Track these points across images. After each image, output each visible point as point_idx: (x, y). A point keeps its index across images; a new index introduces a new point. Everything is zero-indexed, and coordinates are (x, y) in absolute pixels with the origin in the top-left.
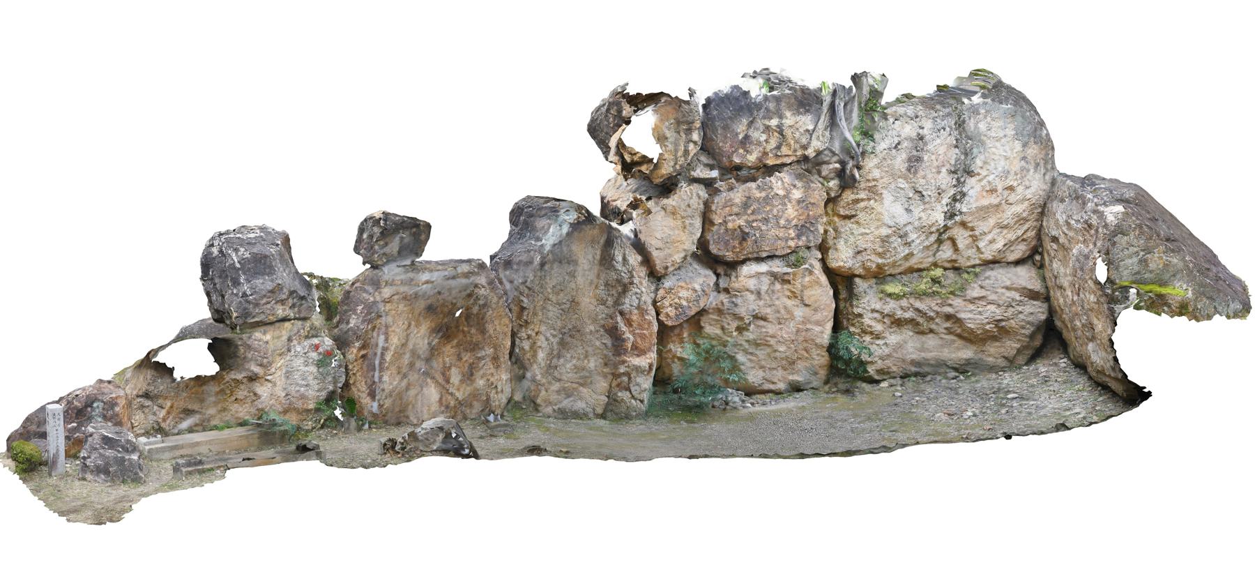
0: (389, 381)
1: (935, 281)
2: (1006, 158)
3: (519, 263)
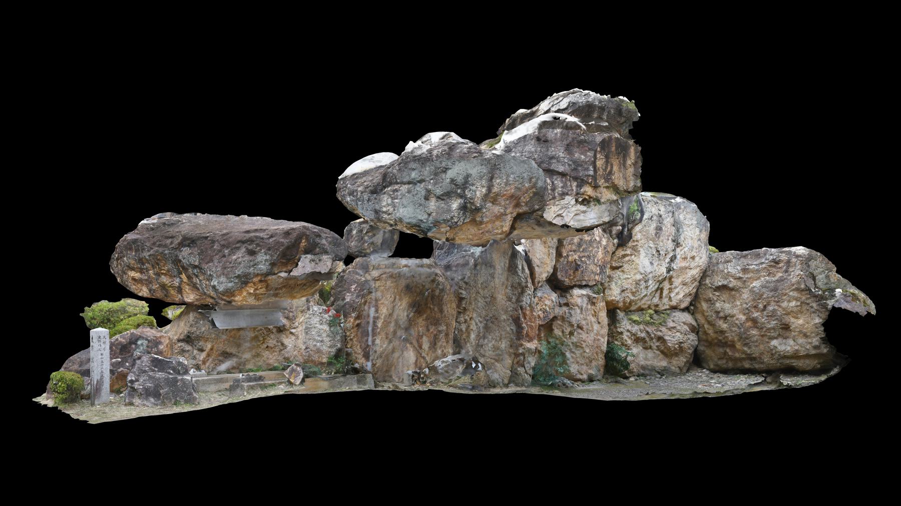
0: (380, 344)
3: (457, 265)
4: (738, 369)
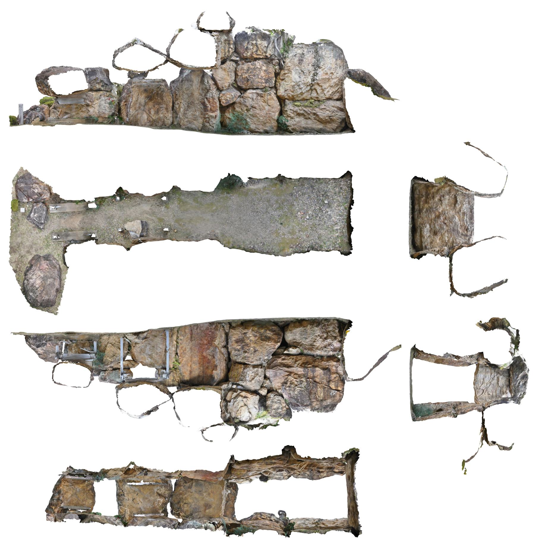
0: (132, 111)
1: (311, 103)
2: (331, 64)
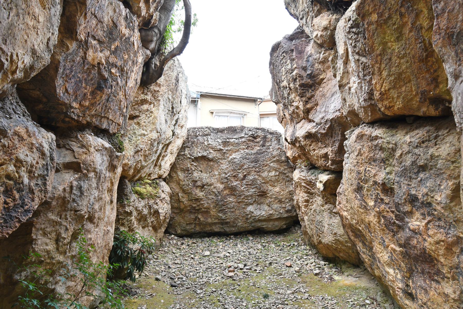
4: (205, 233)
